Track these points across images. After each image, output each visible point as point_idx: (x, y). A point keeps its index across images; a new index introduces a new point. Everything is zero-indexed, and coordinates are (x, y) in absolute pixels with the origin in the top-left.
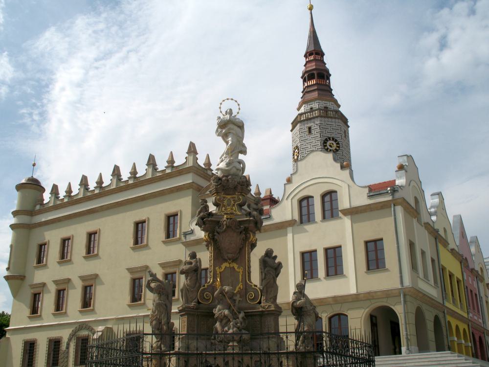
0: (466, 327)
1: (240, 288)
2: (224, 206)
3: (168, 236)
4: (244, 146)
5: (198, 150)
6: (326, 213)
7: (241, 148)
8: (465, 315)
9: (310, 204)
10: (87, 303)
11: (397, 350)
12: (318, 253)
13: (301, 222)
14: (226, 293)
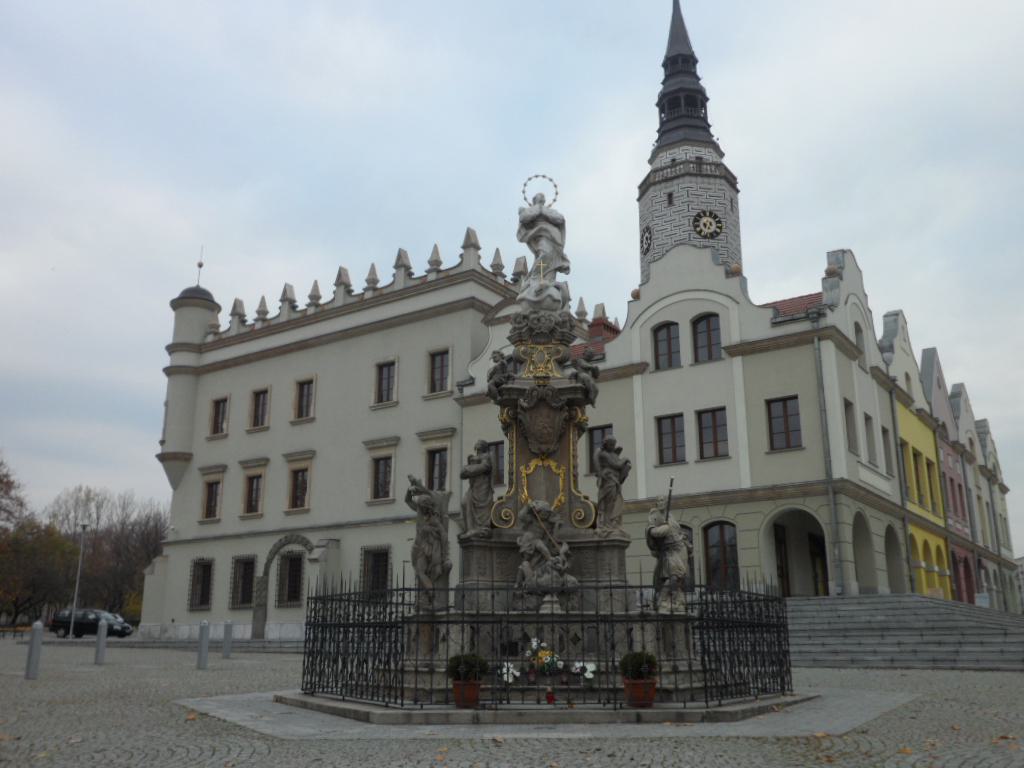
0: (941, 543)
1: (560, 501)
2: (533, 362)
3: (433, 388)
4: (564, 258)
5: (481, 243)
6: (700, 351)
7: (560, 264)
8: (941, 523)
9: (677, 429)
10: (298, 495)
11: (820, 587)
12: (681, 327)
13: (658, 368)
14: (539, 512)
